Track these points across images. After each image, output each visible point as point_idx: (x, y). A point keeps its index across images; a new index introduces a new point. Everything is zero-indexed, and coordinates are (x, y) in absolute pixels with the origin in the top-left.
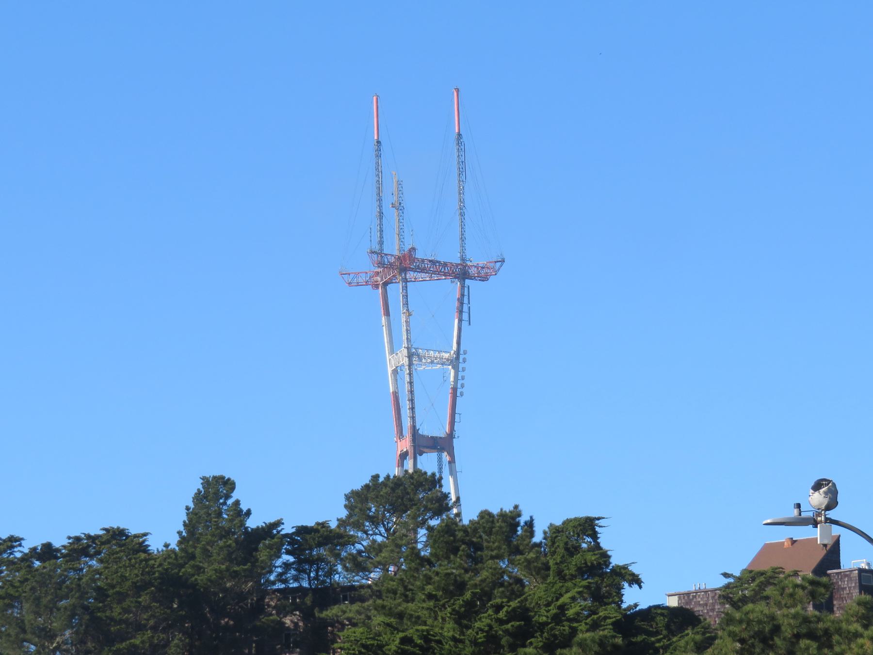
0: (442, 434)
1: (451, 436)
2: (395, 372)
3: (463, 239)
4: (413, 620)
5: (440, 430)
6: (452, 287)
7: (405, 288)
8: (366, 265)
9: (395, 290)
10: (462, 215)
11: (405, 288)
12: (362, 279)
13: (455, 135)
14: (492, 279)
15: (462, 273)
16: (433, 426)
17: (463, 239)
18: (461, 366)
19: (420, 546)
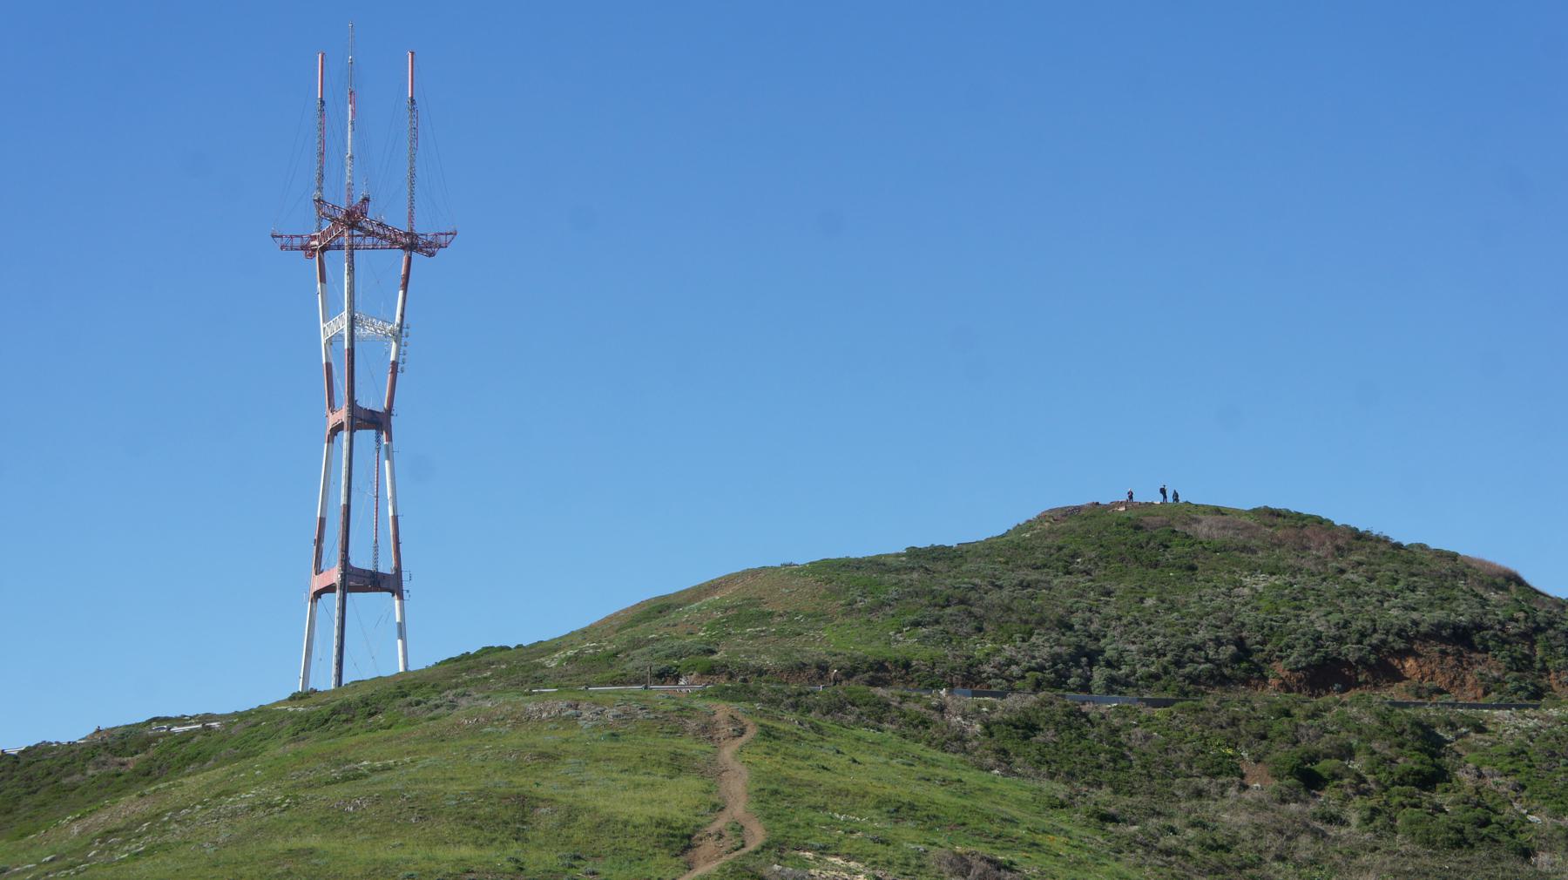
0: (381, 410)
1: (389, 411)
2: (330, 342)
3: (412, 207)
4: (692, 724)
5: (380, 406)
6: (403, 257)
7: (351, 255)
8: (307, 224)
9: (337, 261)
10: (412, 184)
11: (351, 255)
12: (297, 242)
13: (407, 104)
14: (440, 252)
15: (413, 244)
16: (372, 400)
17: (412, 207)
18: (404, 340)
19: (943, 692)
